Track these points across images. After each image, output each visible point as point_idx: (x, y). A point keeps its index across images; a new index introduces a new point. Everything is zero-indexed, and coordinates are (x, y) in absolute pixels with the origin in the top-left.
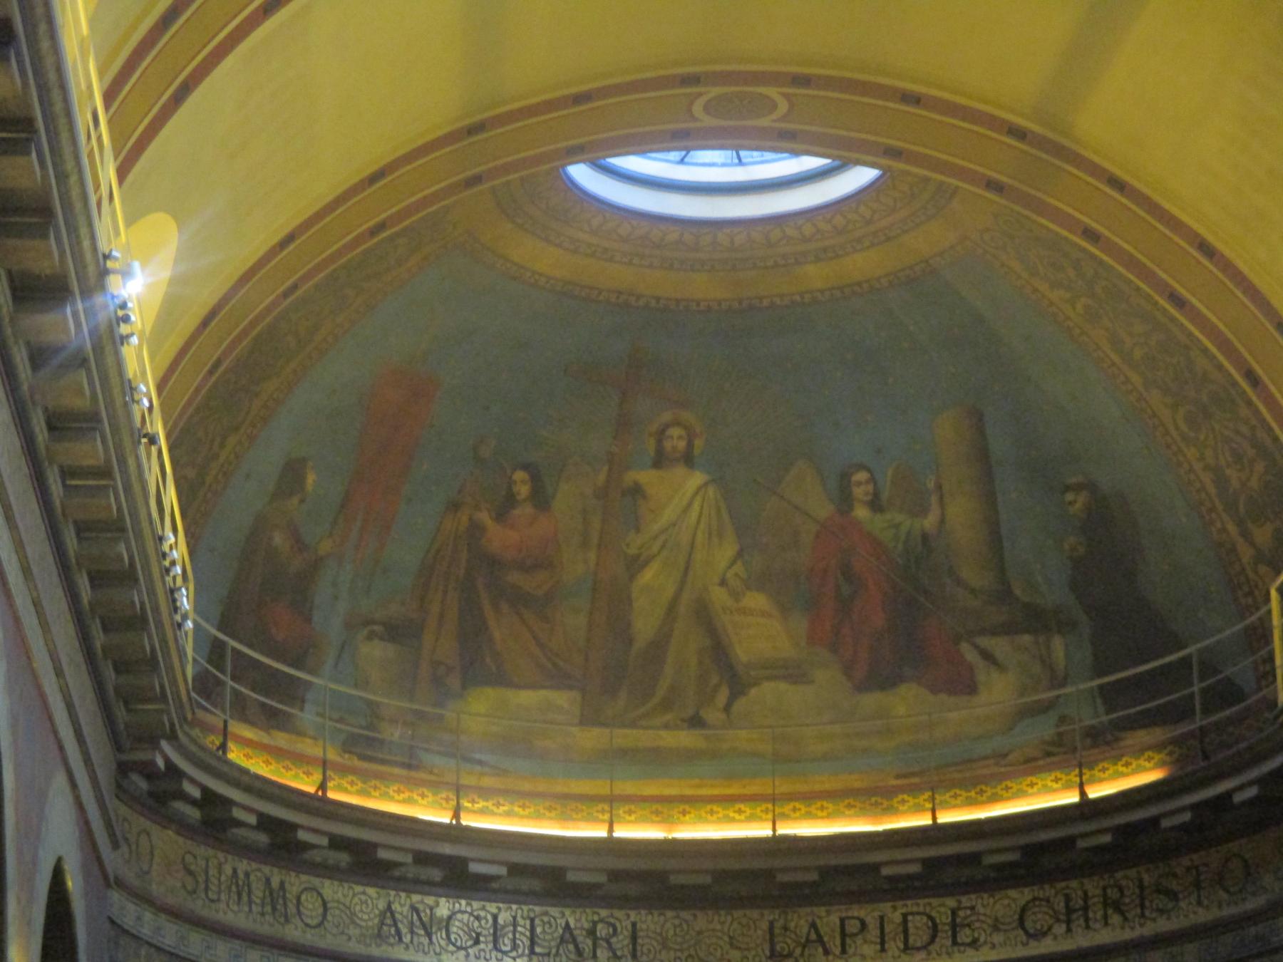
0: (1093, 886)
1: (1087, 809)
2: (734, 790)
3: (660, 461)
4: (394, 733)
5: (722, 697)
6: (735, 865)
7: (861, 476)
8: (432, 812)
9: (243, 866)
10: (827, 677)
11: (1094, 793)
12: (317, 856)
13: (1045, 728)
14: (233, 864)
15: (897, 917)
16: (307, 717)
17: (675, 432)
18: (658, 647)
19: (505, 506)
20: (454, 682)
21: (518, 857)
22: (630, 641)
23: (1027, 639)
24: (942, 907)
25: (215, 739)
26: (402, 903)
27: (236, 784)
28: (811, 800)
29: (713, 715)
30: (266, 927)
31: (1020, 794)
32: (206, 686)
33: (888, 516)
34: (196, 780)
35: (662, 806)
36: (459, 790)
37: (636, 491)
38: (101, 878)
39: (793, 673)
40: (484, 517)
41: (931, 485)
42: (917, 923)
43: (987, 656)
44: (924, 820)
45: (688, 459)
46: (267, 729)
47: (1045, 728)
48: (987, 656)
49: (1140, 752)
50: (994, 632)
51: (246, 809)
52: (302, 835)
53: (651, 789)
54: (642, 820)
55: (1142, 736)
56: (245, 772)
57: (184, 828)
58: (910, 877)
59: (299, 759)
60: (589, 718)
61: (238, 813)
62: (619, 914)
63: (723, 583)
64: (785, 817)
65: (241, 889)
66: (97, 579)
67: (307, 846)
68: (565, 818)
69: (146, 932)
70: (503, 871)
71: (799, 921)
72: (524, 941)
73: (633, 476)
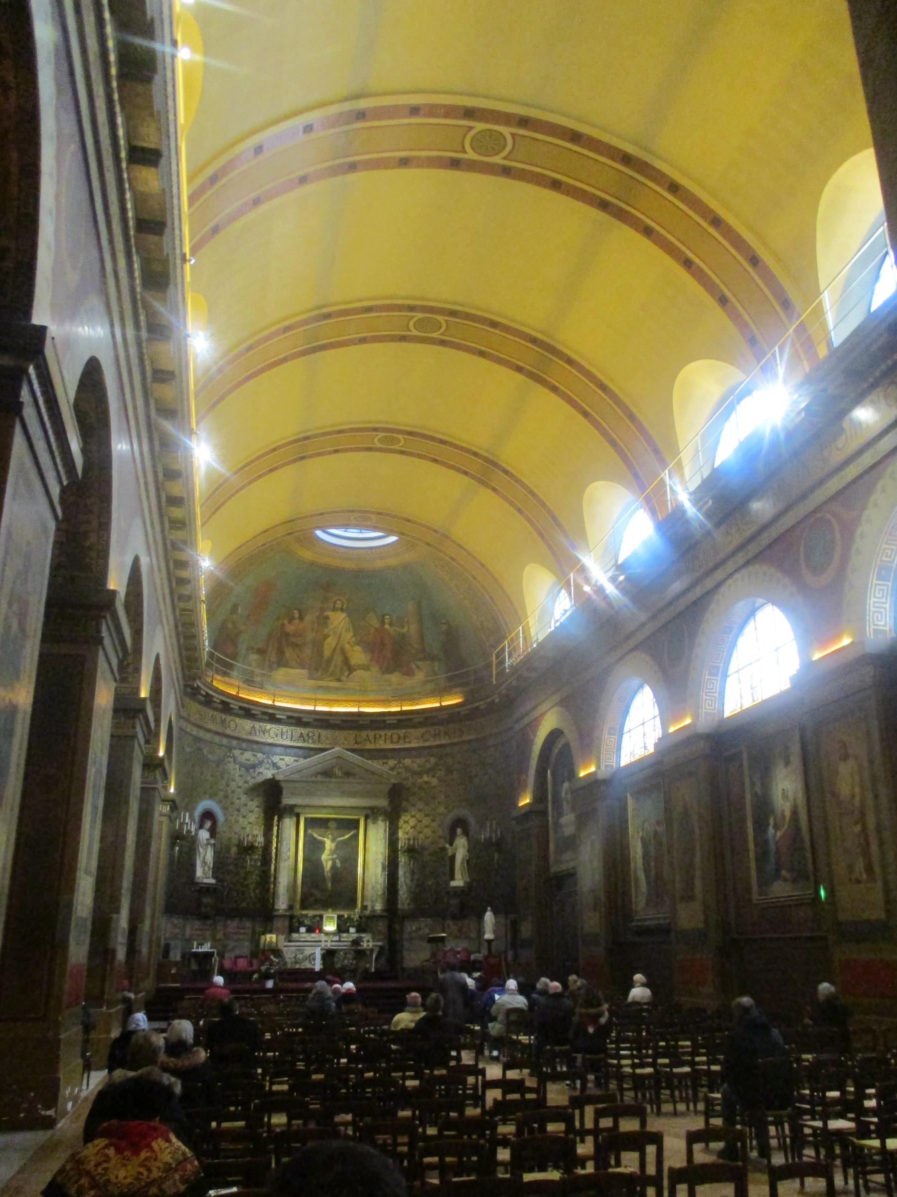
0: (442, 728)
1: (441, 708)
2: (349, 698)
3: (334, 609)
4: (258, 679)
5: (346, 673)
6: (349, 718)
7: (388, 617)
8: (266, 701)
9: (215, 713)
10: (375, 669)
11: (444, 704)
12: (235, 711)
13: (430, 686)
14: (211, 712)
15: (389, 734)
16: (235, 673)
17: (339, 602)
18: (330, 661)
19: (291, 620)
20: (275, 666)
21: (289, 714)
22: (322, 657)
23: (428, 662)
24: (402, 732)
25: (548, 980)
26: (257, 725)
27: (215, 691)
28: (369, 702)
29: (343, 678)
30: (220, 730)
31: (425, 703)
32: (208, 665)
33: (394, 628)
34: (204, 690)
35: (329, 702)
36: (274, 695)
37: (327, 618)
38: (179, 716)
39: (366, 668)
40: (286, 622)
41: (406, 620)
42: (395, 736)
43: (418, 667)
44: (398, 709)
45: (342, 610)
46: (223, 676)
47: (430, 686)
48: (418, 667)
49: (456, 693)
50: (420, 660)
51: (218, 698)
52: (232, 706)
53: (326, 697)
54: (323, 705)
55: (458, 689)
56: (217, 688)
57: (201, 703)
58: (394, 724)
59: (231, 685)
60: (311, 677)
61: (215, 700)
62: (316, 730)
63: (349, 643)
64: (361, 706)
65: (213, 719)
66: (185, 637)
67: (233, 709)
68: (302, 704)
69: (188, 730)
70: (285, 717)
71: (364, 734)
72: (289, 736)
73: (326, 613)
